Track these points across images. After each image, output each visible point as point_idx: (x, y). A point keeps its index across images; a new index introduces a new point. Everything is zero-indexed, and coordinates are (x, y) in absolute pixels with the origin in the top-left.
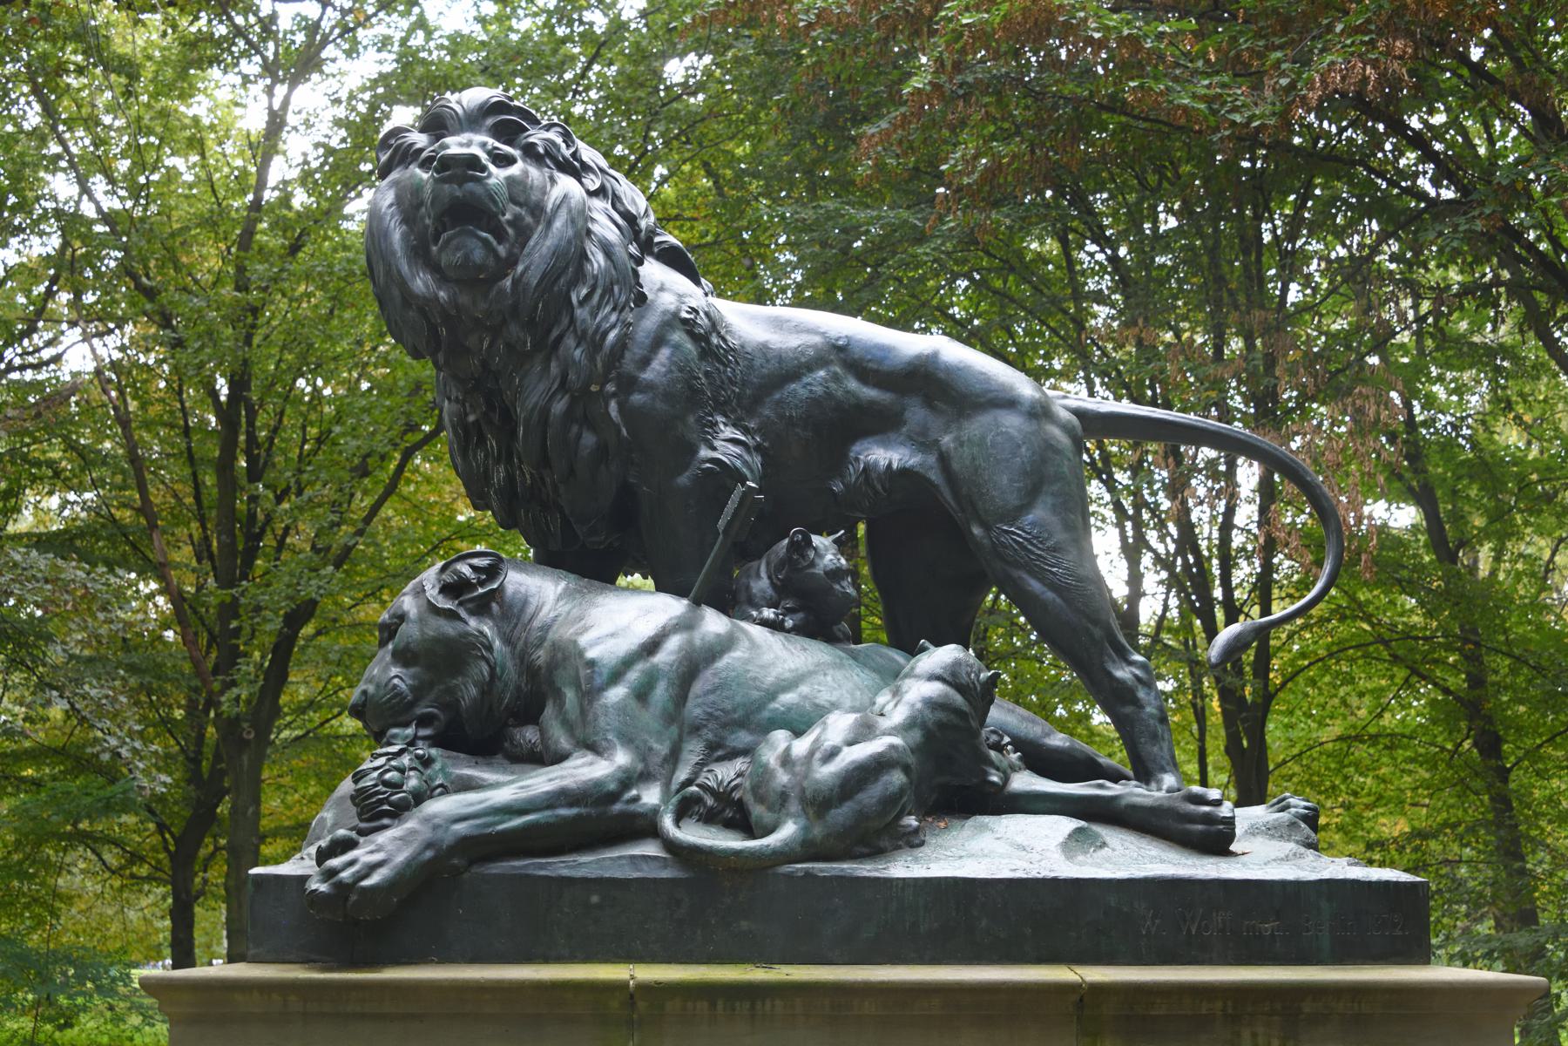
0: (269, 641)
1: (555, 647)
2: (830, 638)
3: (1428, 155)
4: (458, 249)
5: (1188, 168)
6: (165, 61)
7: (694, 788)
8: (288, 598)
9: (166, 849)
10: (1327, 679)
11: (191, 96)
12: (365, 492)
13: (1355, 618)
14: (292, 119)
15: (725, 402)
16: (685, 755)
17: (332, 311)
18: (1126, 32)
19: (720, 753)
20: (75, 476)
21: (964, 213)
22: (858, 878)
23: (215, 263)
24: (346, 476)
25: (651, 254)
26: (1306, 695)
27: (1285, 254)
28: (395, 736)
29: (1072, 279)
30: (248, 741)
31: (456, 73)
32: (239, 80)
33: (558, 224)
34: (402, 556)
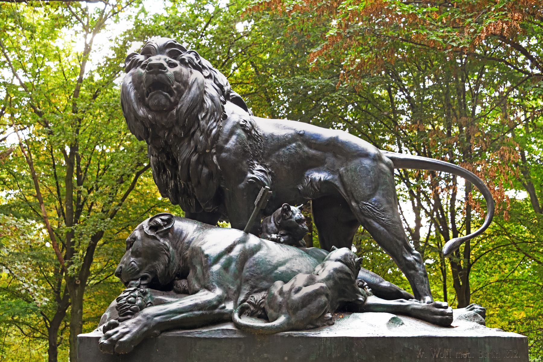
0: (86, 247)
1: (193, 249)
2: (298, 246)
3: (528, 56)
4: (155, 99)
5: (436, 62)
6: (46, 26)
7: (246, 303)
8: (93, 230)
9: (47, 326)
10: (493, 258)
11: (55, 39)
12: (122, 189)
13: (503, 235)
14: (93, 48)
15: (257, 156)
16: (243, 291)
17: (109, 120)
18: (411, 12)
19: (256, 290)
20: (11, 184)
21: (351, 80)
22: (309, 337)
23: (64, 102)
24: (115, 183)
25: (229, 100)
26: (485, 264)
27: (474, 95)
28: (132, 284)
29: (393, 106)
30: (78, 285)
31: (156, 29)
32: (74, 33)
33: (194, 89)
34: (136, 213)
